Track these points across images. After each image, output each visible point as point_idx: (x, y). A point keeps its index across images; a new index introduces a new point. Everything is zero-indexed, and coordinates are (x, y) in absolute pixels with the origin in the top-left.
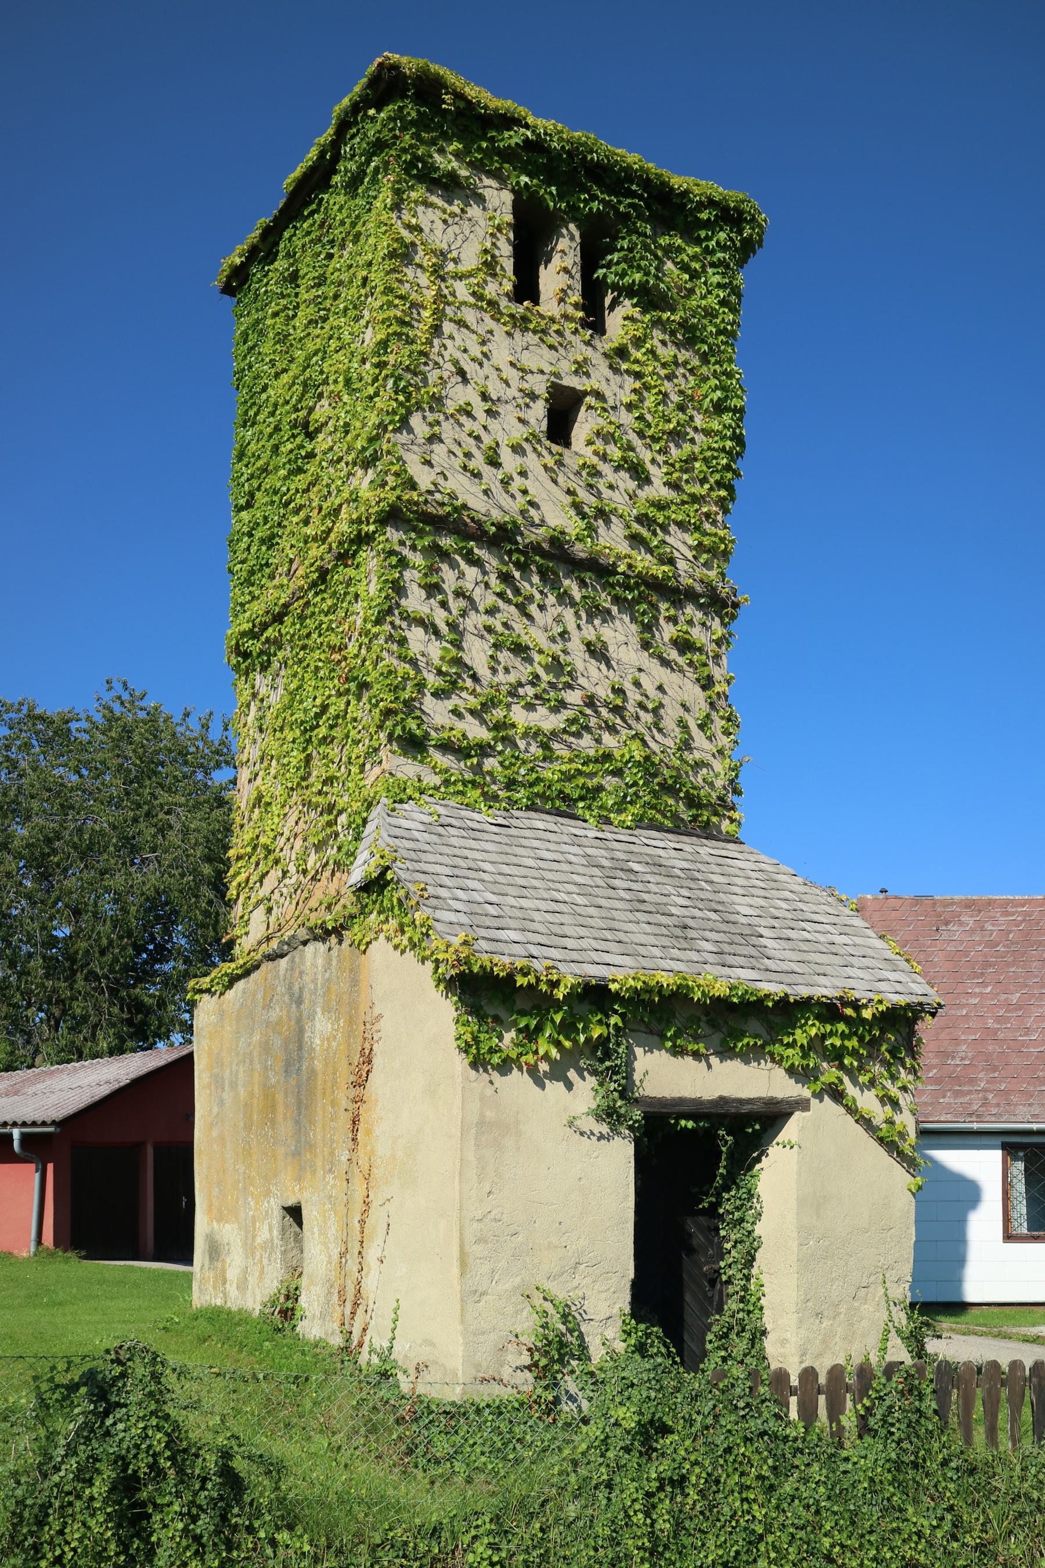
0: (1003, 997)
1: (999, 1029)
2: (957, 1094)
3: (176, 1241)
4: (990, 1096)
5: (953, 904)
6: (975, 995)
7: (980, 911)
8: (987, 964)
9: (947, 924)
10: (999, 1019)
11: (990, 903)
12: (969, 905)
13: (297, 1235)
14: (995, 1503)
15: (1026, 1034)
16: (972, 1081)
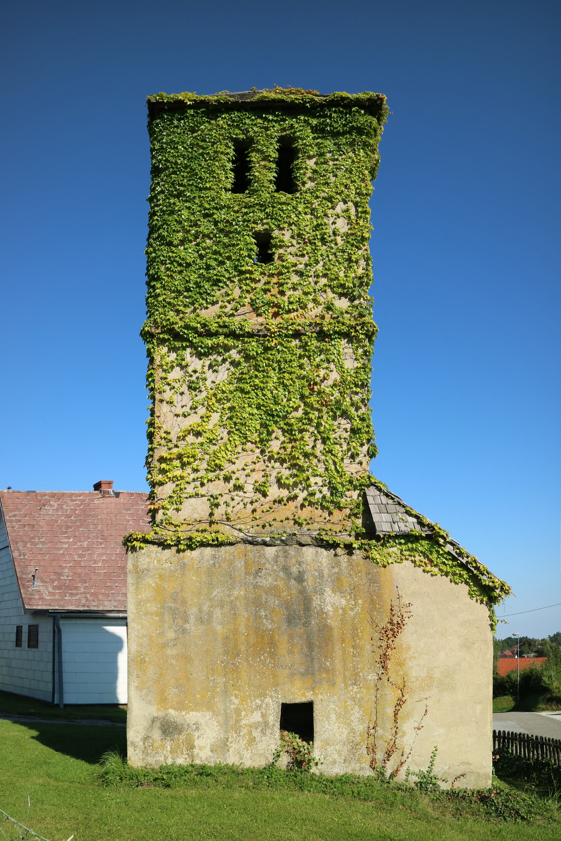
0: (79, 544)
1: (81, 561)
2: (71, 595)
3: (120, 746)
4: (88, 596)
5: (45, 495)
6: (65, 543)
7: (59, 499)
8: (68, 527)
9: (44, 505)
10: (80, 556)
11: (63, 494)
12: (53, 495)
13: (505, 708)
14: (53, 786)
15: (95, 563)
16: (76, 588)
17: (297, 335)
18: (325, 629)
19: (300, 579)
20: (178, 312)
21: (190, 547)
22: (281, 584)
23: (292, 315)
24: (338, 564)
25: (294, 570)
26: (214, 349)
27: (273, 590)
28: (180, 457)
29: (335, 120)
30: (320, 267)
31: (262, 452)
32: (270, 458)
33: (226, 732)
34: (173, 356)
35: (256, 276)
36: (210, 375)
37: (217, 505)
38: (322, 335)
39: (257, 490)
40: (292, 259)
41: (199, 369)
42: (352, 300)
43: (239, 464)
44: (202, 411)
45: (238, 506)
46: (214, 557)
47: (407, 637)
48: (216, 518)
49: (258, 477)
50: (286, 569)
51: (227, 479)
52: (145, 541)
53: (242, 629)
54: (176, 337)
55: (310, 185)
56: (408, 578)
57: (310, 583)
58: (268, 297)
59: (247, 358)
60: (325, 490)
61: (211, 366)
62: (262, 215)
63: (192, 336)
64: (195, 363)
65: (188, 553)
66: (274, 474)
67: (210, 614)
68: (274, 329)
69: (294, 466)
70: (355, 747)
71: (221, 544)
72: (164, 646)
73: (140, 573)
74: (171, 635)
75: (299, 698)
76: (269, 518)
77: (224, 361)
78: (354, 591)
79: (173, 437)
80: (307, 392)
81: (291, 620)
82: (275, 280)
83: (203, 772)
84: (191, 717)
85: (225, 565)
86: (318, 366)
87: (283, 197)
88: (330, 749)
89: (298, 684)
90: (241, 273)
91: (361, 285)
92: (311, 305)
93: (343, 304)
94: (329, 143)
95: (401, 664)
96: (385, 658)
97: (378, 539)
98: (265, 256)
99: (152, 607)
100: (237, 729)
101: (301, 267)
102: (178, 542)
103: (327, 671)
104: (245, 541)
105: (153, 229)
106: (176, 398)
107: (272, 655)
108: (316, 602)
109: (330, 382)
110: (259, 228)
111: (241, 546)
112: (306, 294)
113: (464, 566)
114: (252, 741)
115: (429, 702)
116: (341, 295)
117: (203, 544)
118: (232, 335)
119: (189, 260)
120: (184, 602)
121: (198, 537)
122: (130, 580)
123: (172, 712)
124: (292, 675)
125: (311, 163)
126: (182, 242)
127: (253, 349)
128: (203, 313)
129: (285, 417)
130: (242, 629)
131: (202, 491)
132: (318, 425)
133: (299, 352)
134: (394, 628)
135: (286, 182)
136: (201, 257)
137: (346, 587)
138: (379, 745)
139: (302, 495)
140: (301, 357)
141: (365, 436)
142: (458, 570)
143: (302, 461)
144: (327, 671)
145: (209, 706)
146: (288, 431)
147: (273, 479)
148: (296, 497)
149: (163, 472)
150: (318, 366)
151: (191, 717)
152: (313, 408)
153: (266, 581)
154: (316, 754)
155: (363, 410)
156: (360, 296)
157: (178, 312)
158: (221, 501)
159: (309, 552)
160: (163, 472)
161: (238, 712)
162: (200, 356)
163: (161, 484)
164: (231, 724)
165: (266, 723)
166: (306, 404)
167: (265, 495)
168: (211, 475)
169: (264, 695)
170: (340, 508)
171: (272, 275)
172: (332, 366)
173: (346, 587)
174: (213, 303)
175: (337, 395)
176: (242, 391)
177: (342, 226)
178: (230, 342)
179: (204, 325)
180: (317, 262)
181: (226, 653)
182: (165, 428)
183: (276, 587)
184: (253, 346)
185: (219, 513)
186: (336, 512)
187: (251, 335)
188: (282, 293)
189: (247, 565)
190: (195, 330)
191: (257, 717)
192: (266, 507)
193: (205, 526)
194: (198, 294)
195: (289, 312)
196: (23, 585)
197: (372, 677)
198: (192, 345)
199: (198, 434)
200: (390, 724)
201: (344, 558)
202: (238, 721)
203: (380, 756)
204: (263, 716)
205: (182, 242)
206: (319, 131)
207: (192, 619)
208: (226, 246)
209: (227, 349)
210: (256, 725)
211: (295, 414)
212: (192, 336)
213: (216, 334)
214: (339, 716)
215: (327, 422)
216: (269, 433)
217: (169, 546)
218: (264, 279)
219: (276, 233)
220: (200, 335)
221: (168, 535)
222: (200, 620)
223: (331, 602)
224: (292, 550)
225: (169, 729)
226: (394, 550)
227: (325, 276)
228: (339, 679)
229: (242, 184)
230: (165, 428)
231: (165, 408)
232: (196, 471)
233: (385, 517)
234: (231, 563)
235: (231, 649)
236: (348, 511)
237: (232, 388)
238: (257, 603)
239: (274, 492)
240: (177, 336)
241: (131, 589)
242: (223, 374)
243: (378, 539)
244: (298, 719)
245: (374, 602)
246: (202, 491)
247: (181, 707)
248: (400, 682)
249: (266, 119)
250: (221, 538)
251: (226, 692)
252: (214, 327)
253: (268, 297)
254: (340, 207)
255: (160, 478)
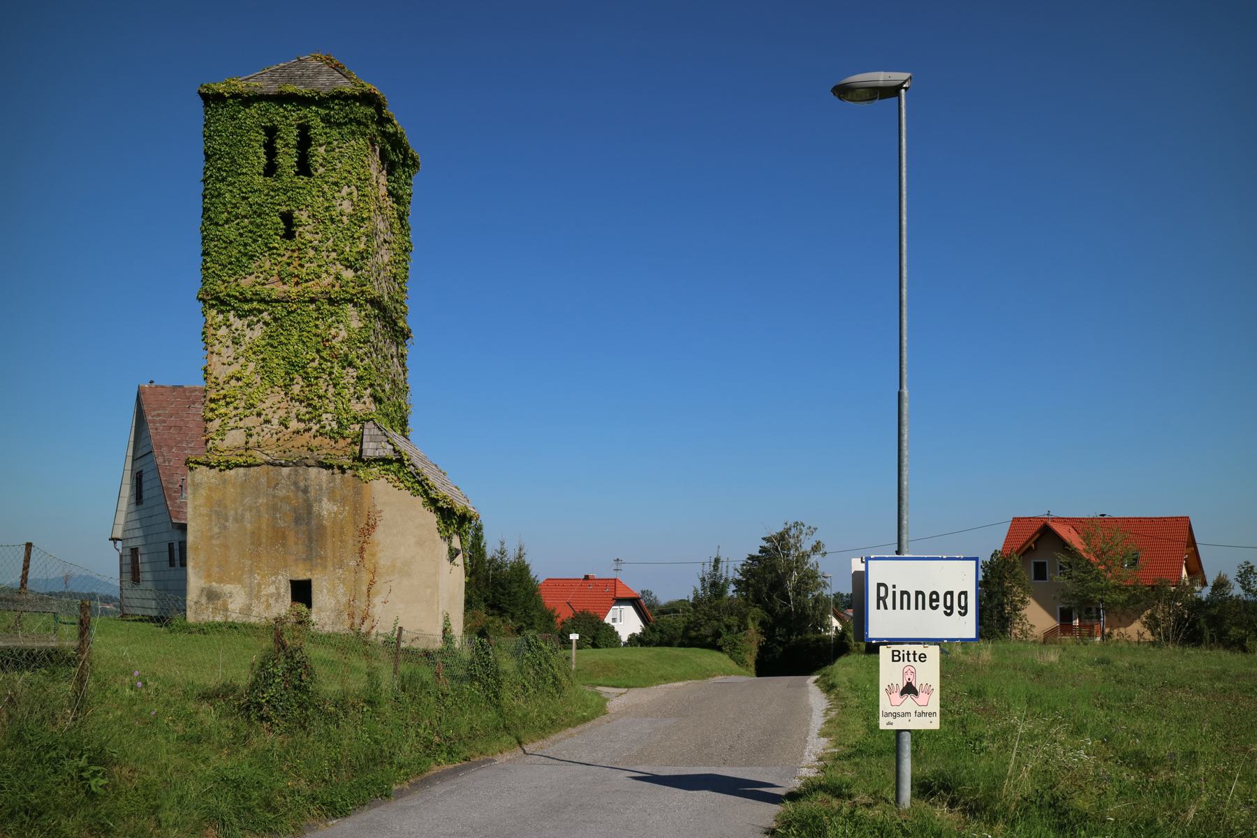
17: (312, 301)
18: (321, 527)
19: (305, 491)
20: (224, 281)
21: (228, 467)
22: (291, 494)
23: (310, 284)
24: (334, 480)
25: (302, 484)
26: (251, 311)
27: (286, 499)
28: (225, 397)
29: (337, 113)
30: (330, 243)
31: (286, 394)
32: (292, 399)
33: (251, 599)
34: (221, 317)
35: (282, 251)
36: (248, 332)
37: (251, 435)
38: (332, 302)
39: (281, 424)
40: (308, 237)
41: (240, 327)
42: (356, 271)
43: (268, 403)
44: (242, 361)
45: (265, 435)
46: (245, 475)
47: (379, 535)
48: (250, 445)
49: (282, 413)
50: (296, 484)
51: (259, 415)
52: (198, 463)
53: (264, 526)
54: (221, 303)
55: (321, 170)
56: (384, 492)
57: (312, 494)
58: (291, 269)
59: (275, 319)
60: (334, 425)
61: (249, 326)
62: (284, 198)
63: (233, 301)
64: (237, 323)
65: (227, 472)
66: (295, 411)
67: (243, 516)
68: (293, 296)
69: (309, 405)
70: (340, 613)
71: (250, 466)
72: (211, 538)
73: (196, 486)
74: (216, 530)
75: (302, 576)
76: (289, 445)
77: (258, 321)
78: (344, 501)
79: (220, 381)
80: (321, 347)
81: (297, 520)
82: (296, 255)
83: (233, 626)
84: (228, 588)
85: (253, 481)
86: (330, 326)
87: (301, 181)
88: (323, 614)
89: (301, 566)
90: (270, 249)
91: (363, 258)
92: (324, 275)
93: (348, 274)
94: (335, 132)
95: (373, 555)
96: (362, 550)
97: (363, 461)
98: (289, 235)
99: (204, 510)
100: (258, 597)
101: (316, 243)
102: (219, 464)
103: (321, 558)
104: (268, 463)
105: (206, 210)
106: (223, 350)
107: (283, 545)
108: (315, 508)
109: (340, 339)
110: (284, 209)
111: (265, 467)
112: (320, 266)
113: (420, 483)
114: (269, 606)
115: (393, 584)
116: (347, 267)
117: (237, 466)
118: (262, 301)
119: (232, 237)
120: (225, 507)
121: (233, 460)
122: (189, 491)
123: (214, 584)
124: (297, 560)
125: (322, 150)
126: (227, 222)
127: (279, 313)
128: (243, 282)
129: (303, 367)
130: (264, 526)
131: (241, 424)
132: (331, 374)
133: (315, 315)
134: (370, 528)
135: (304, 168)
136: (241, 235)
137: (338, 497)
138: (357, 613)
139: (315, 428)
140: (317, 319)
141: (368, 382)
142: (416, 486)
143: (316, 402)
144: (321, 558)
145: (239, 580)
146: (306, 377)
147: (293, 415)
148: (310, 429)
149: (212, 410)
150: (330, 326)
151: (228, 588)
152: (326, 360)
153: (282, 493)
154: (314, 618)
155: (367, 361)
156: (362, 268)
157: (224, 281)
158: (253, 431)
159: (313, 471)
160: (212, 410)
161: (259, 585)
162: (240, 317)
163: (211, 420)
164: (254, 594)
165: (279, 594)
166: (322, 357)
167: (287, 428)
168: (247, 412)
169: (277, 574)
170: (344, 438)
171: (293, 251)
172: (341, 326)
173: (338, 497)
174: (251, 274)
175: (345, 348)
176: (272, 346)
177: (347, 207)
178: (263, 306)
179: (241, 294)
180: (328, 239)
181: (252, 543)
182: (215, 374)
183: (288, 497)
184: (279, 310)
185: (253, 440)
186: (341, 441)
187: (277, 301)
188: (302, 266)
189: (268, 481)
190: (235, 297)
191: (272, 589)
192: (287, 437)
193: (242, 451)
194: (238, 266)
195: (306, 281)
196: (170, 496)
197: (353, 563)
198: (234, 309)
199: (238, 379)
200: (364, 599)
201: (338, 476)
202: (259, 592)
203: (357, 621)
204: (277, 588)
205: (227, 222)
206: (326, 120)
207: (231, 519)
208: (258, 226)
209: (261, 312)
210: (271, 595)
211: (312, 364)
212: (233, 301)
213: (251, 300)
214: (329, 591)
215: (337, 369)
216: (292, 380)
217: (213, 467)
218: (288, 254)
219: (296, 214)
220: (240, 301)
221: (213, 459)
222: (236, 520)
223: (326, 508)
224: (301, 470)
225: (212, 596)
226: (375, 470)
227: (334, 250)
228: (330, 564)
229: (271, 170)
230: (215, 374)
231: (215, 358)
232: (236, 408)
233: (372, 445)
234: (257, 479)
235: (256, 542)
236: (349, 440)
237: (263, 343)
238: (274, 508)
239: (294, 425)
240: (223, 303)
241: (190, 497)
242: (258, 332)
243: (363, 461)
244: (302, 592)
245: (356, 509)
246: (241, 424)
247: (220, 581)
248: (372, 568)
249: (285, 109)
250: (250, 460)
251: (251, 572)
252: (249, 296)
253: (291, 269)
254: (345, 190)
255: (210, 415)
